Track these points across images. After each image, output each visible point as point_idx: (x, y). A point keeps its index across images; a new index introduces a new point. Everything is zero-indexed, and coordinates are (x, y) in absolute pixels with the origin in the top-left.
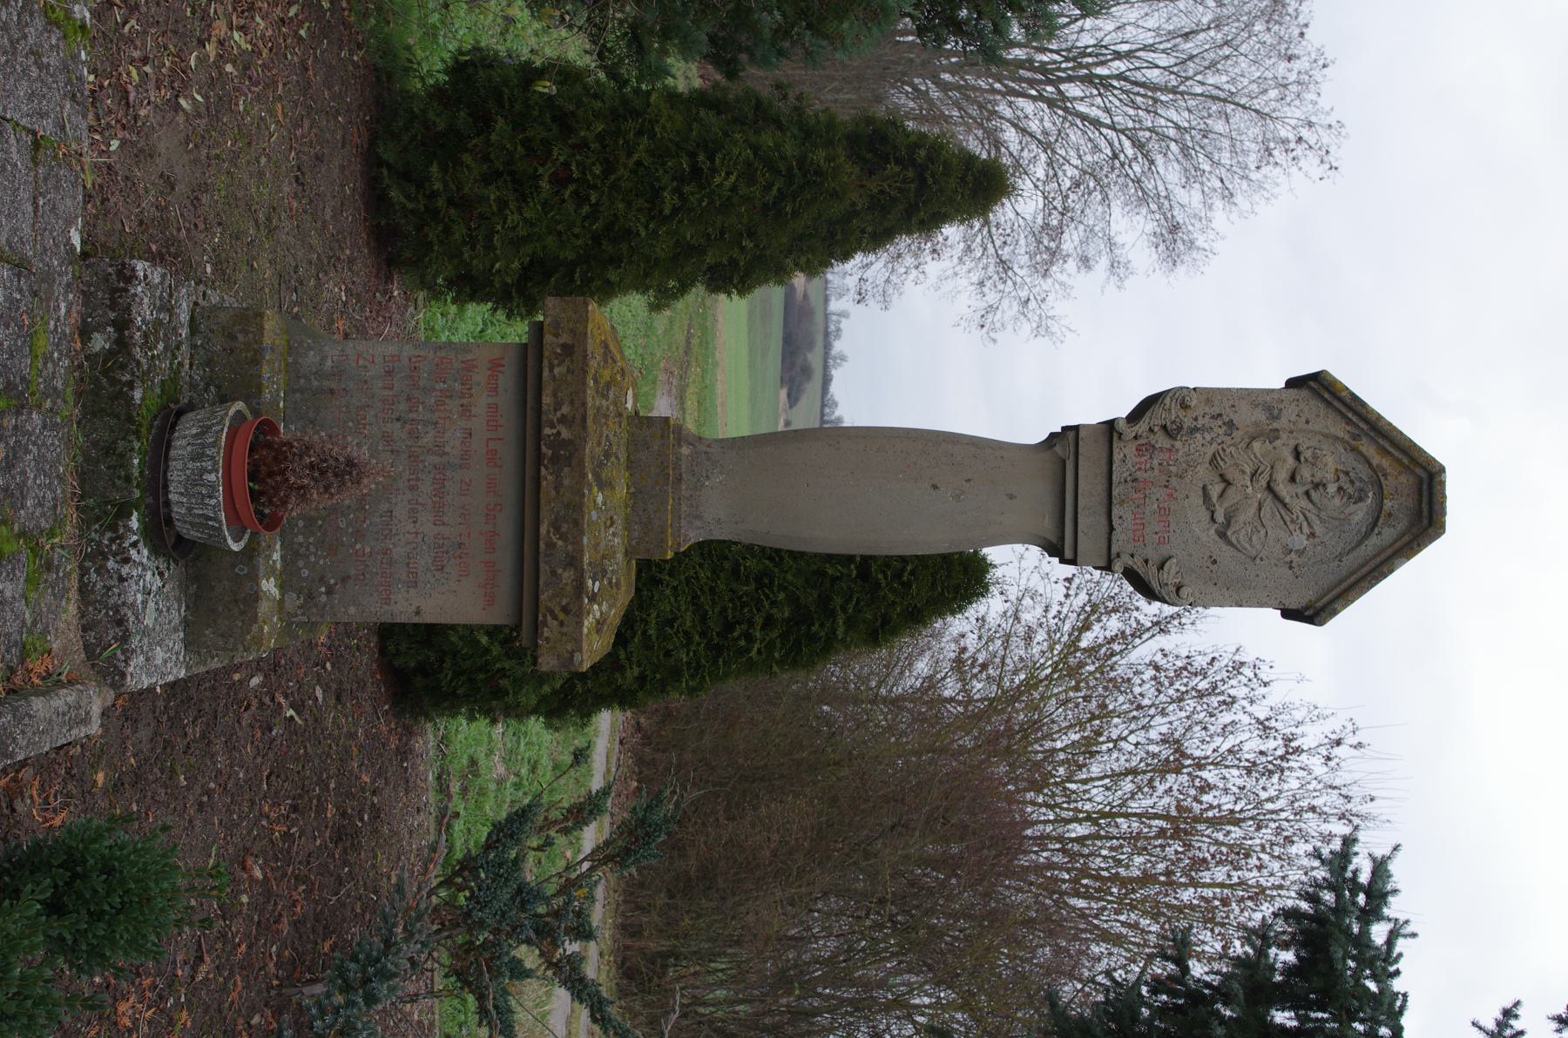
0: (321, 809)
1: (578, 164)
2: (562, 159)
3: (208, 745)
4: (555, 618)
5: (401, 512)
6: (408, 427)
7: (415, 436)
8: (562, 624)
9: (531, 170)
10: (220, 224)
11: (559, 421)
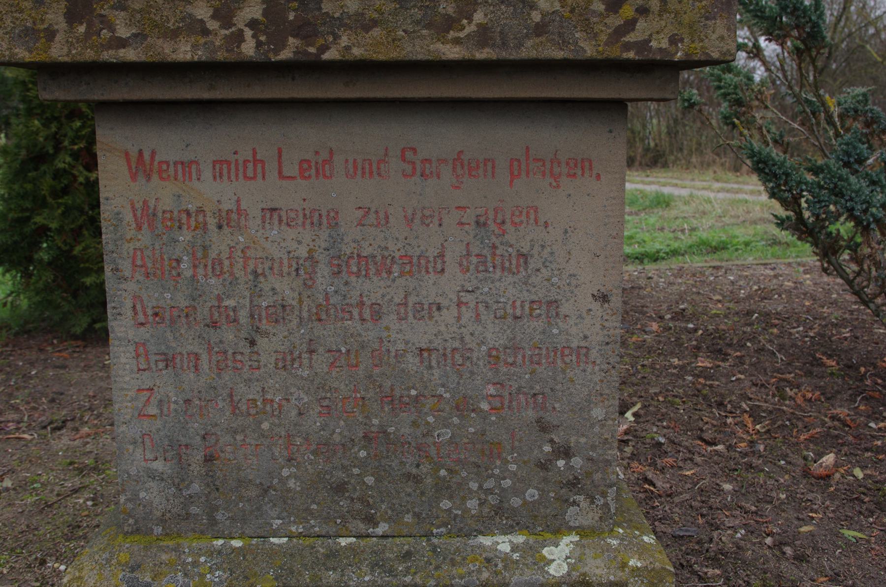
0: (704, 373)
1: (73, 143)
2: (68, 159)
3: (725, 554)
4: (630, 25)
5: (421, 333)
6: (264, 325)
7: (280, 312)
8: (643, 11)
9: (82, 188)
10: (43, 562)
11: (227, 23)
